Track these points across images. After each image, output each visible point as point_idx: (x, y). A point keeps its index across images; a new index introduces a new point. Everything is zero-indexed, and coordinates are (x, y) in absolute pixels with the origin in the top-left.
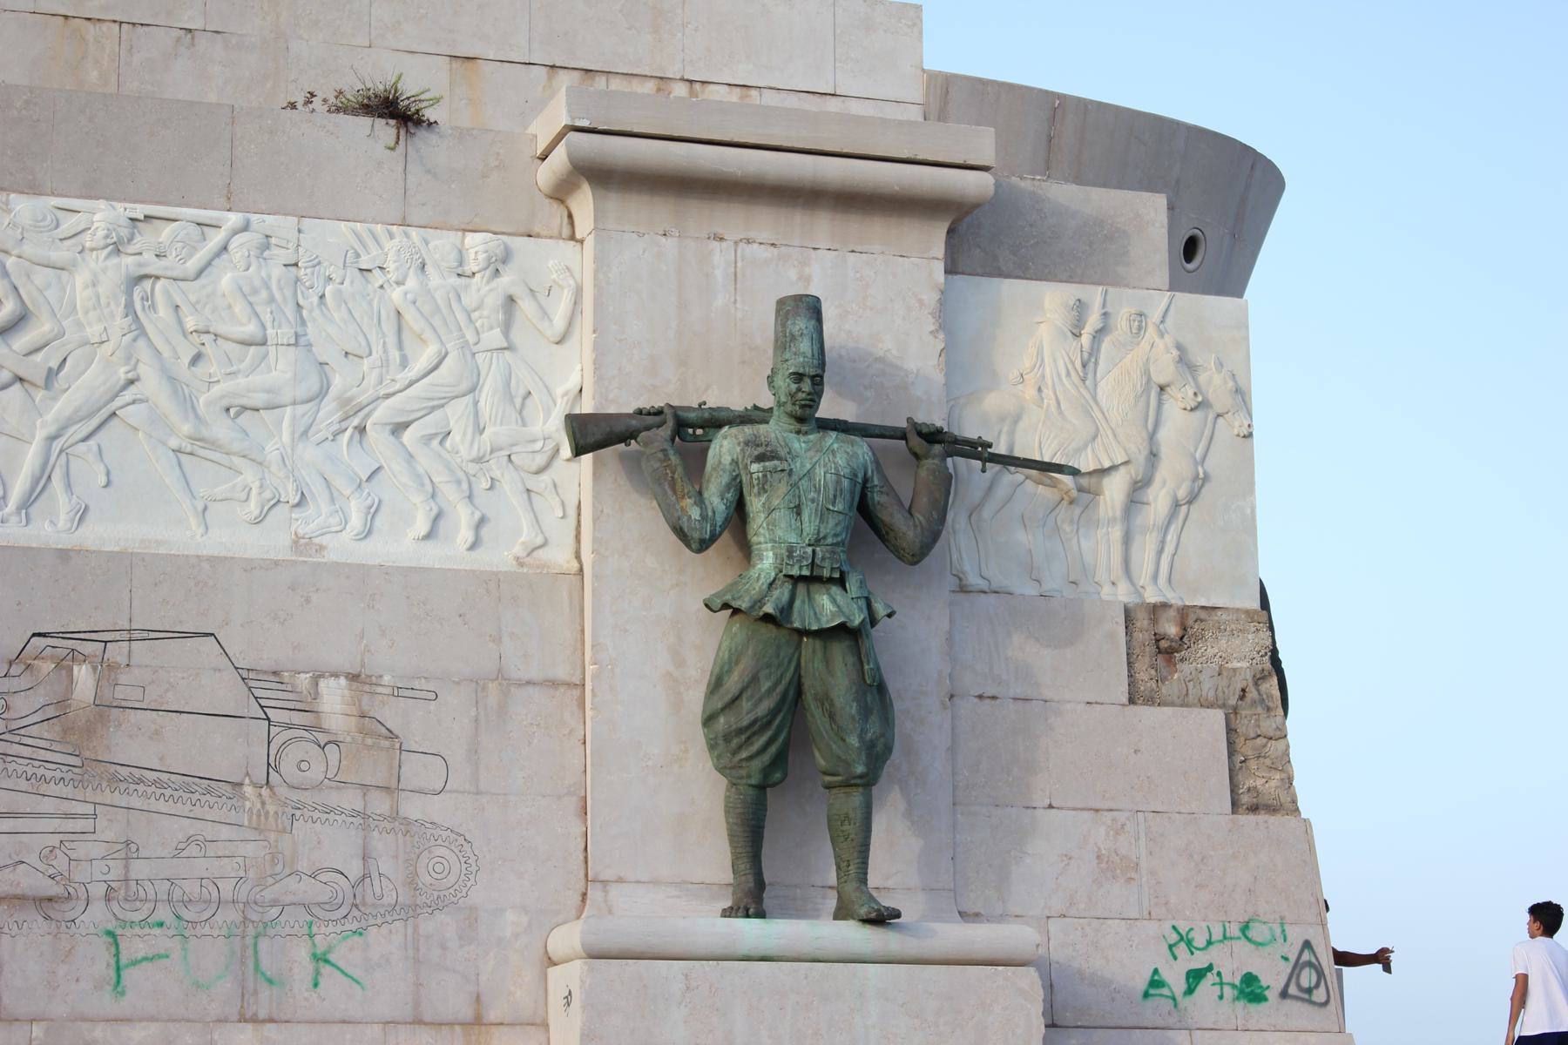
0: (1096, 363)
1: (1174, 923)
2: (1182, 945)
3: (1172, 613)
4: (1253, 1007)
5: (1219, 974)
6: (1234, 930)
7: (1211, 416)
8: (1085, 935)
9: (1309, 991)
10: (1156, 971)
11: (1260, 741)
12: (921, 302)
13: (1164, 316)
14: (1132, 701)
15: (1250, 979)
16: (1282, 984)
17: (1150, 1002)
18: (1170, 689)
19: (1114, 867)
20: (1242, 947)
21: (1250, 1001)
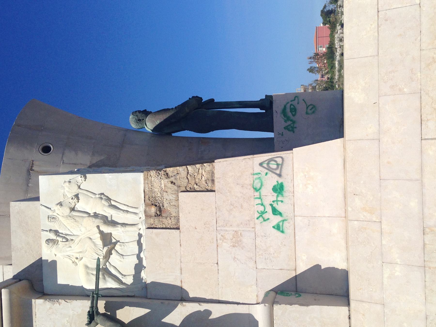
0: (66, 235)
1: (256, 218)
2: (264, 216)
3: (147, 209)
4: (285, 189)
5: (273, 202)
6: (257, 194)
7: (80, 191)
8: (262, 255)
9: (278, 165)
10: (274, 227)
11: (189, 177)
12: (50, 308)
13: (48, 208)
14: (178, 228)
15: (275, 189)
16: (276, 176)
17: (285, 230)
18: (173, 211)
19: (237, 242)
20: (264, 191)
21: (283, 190)
